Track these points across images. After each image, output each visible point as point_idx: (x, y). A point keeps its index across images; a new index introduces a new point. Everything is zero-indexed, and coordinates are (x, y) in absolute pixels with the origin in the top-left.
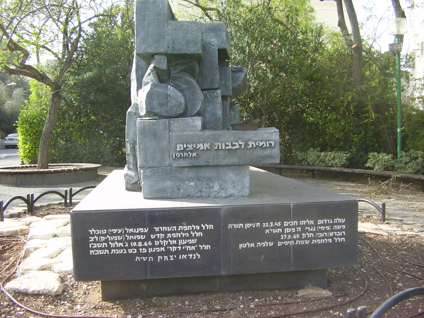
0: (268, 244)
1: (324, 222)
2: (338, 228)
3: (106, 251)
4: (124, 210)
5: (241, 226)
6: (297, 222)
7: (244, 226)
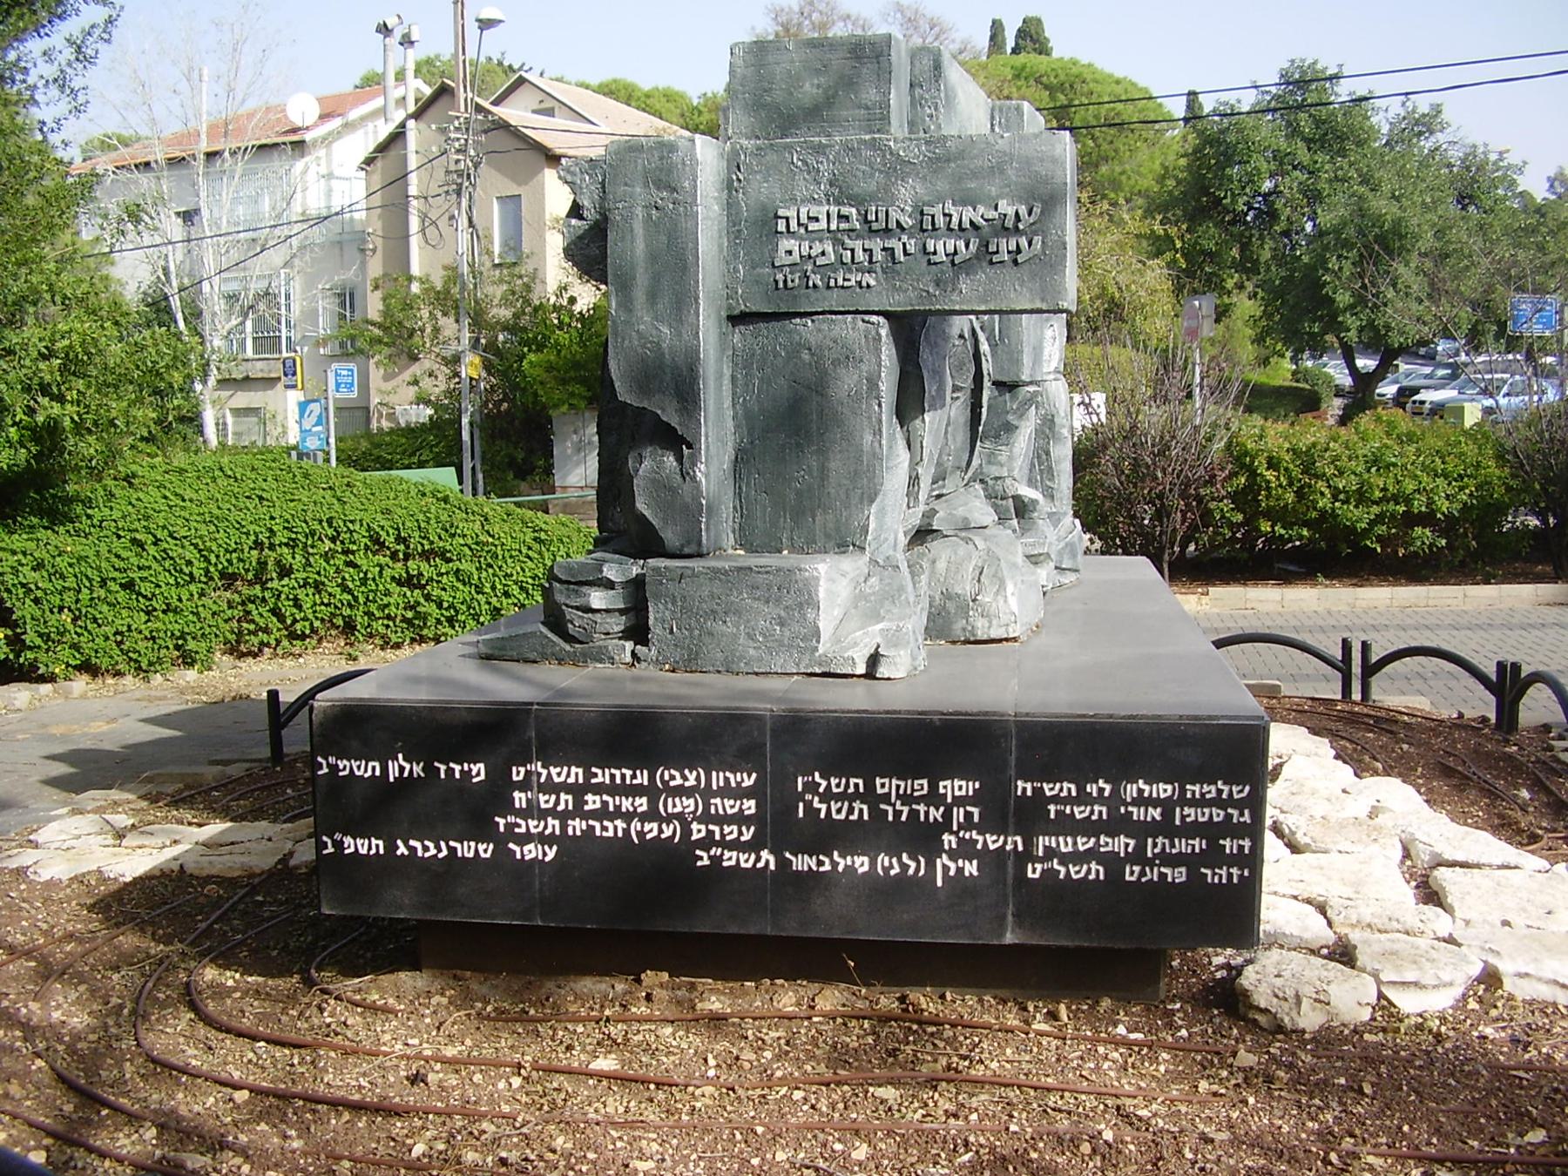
0: (985, 841)
1: (613, 776)
2: (730, 811)
3: (857, 805)
4: (1154, 717)
5: (856, 785)
6: (580, 771)
7: (385, 769)
